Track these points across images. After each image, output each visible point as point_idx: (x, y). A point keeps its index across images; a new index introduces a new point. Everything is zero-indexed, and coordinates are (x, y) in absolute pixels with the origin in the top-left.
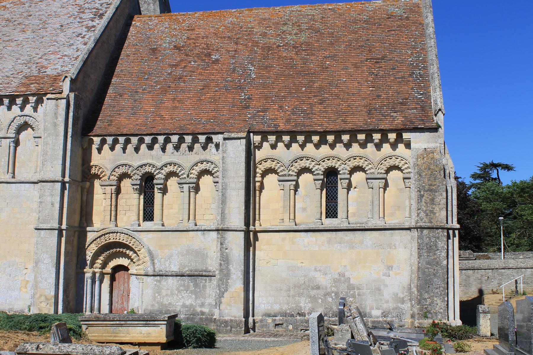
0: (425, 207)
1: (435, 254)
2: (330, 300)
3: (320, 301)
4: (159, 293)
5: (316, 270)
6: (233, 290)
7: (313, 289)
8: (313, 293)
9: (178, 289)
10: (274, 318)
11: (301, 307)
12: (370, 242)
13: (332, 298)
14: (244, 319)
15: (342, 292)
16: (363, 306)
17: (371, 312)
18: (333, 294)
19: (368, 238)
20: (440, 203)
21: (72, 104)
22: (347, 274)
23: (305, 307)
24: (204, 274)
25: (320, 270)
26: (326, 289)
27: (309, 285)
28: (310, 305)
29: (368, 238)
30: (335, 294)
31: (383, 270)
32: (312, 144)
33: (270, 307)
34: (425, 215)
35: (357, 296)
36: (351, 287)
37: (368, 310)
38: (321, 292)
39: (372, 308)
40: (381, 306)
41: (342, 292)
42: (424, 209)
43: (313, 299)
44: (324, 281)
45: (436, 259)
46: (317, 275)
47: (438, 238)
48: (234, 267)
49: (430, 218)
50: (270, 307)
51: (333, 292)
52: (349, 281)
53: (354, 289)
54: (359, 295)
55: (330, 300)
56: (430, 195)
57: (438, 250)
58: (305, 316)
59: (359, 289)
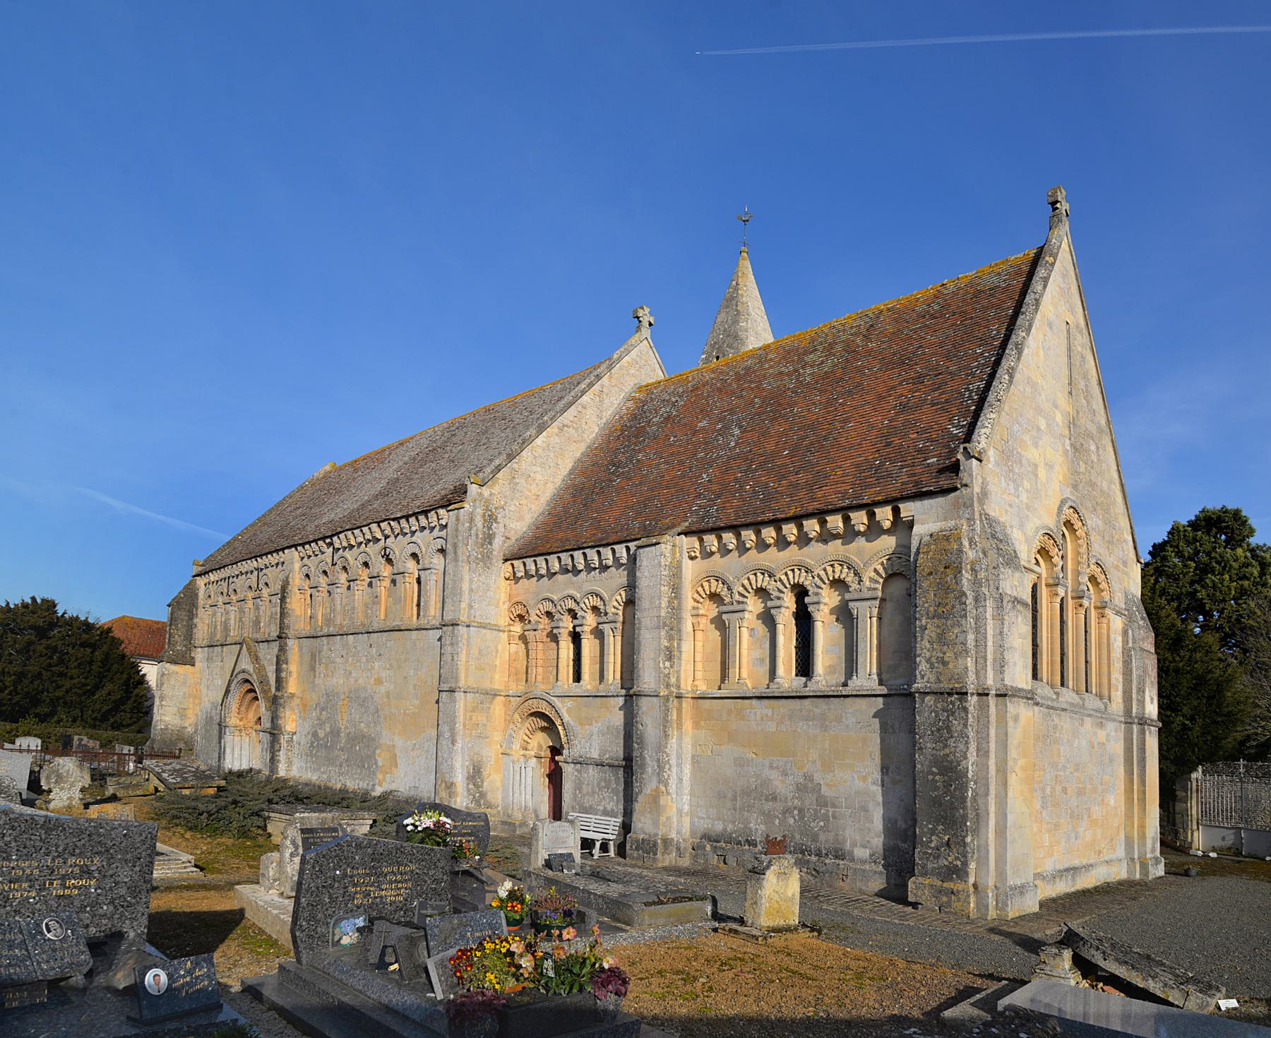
0: (928, 651)
1: (946, 746)
2: (791, 821)
3: (777, 822)
4: (580, 789)
5: (771, 767)
6: (649, 792)
7: (767, 800)
8: (768, 806)
9: (598, 785)
10: (715, 844)
11: (750, 829)
12: (854, 720)
13: (794, 819)
14: (378, 791)
15: (808, 809)
16: (840, 838)
17: (853, 851)
18: (796, 812)
19: (850, 711)
20: (957, 641)
21: (1118, 646)
22: (818, 777)
23: (757, 829)
24: (445, 728)
25: (777, 768)
26: (786, 802)
27: (762, 792)
28: (763, 827)
29: (850, 711)
30: (800, 812)
31: (873, 773)
32: (792, 545)
33: (710, 826)
34: (928, 666)
35: (831, 819)
36: (823, 802)
37: (848, 846)
38: (779, 806)
39: (854, 844)
40: (868, 842)
41: (808, 809)
42: (928, 654)
43: (768, 817)
44: (783, 786)
45: (947, 755)
46: (774, 775)
47: (953, 713)
48: (650, 753)
49: (937, 672)
50: (710, 826)
51: (795, 808)
52: (820, 789)
53: (827, 806)
54: (834, 817)
55: (791, 821)
56: (938, 627)
57: (952, 737)
58: (756, 846)
59: (834, 806)
